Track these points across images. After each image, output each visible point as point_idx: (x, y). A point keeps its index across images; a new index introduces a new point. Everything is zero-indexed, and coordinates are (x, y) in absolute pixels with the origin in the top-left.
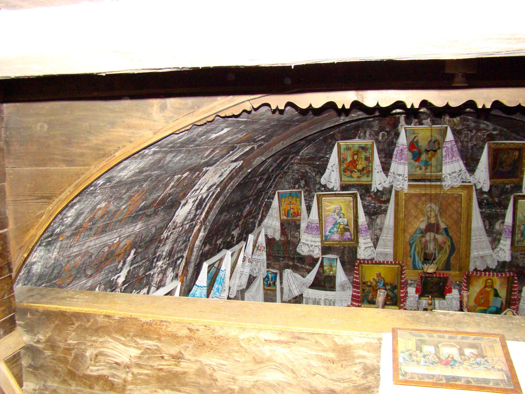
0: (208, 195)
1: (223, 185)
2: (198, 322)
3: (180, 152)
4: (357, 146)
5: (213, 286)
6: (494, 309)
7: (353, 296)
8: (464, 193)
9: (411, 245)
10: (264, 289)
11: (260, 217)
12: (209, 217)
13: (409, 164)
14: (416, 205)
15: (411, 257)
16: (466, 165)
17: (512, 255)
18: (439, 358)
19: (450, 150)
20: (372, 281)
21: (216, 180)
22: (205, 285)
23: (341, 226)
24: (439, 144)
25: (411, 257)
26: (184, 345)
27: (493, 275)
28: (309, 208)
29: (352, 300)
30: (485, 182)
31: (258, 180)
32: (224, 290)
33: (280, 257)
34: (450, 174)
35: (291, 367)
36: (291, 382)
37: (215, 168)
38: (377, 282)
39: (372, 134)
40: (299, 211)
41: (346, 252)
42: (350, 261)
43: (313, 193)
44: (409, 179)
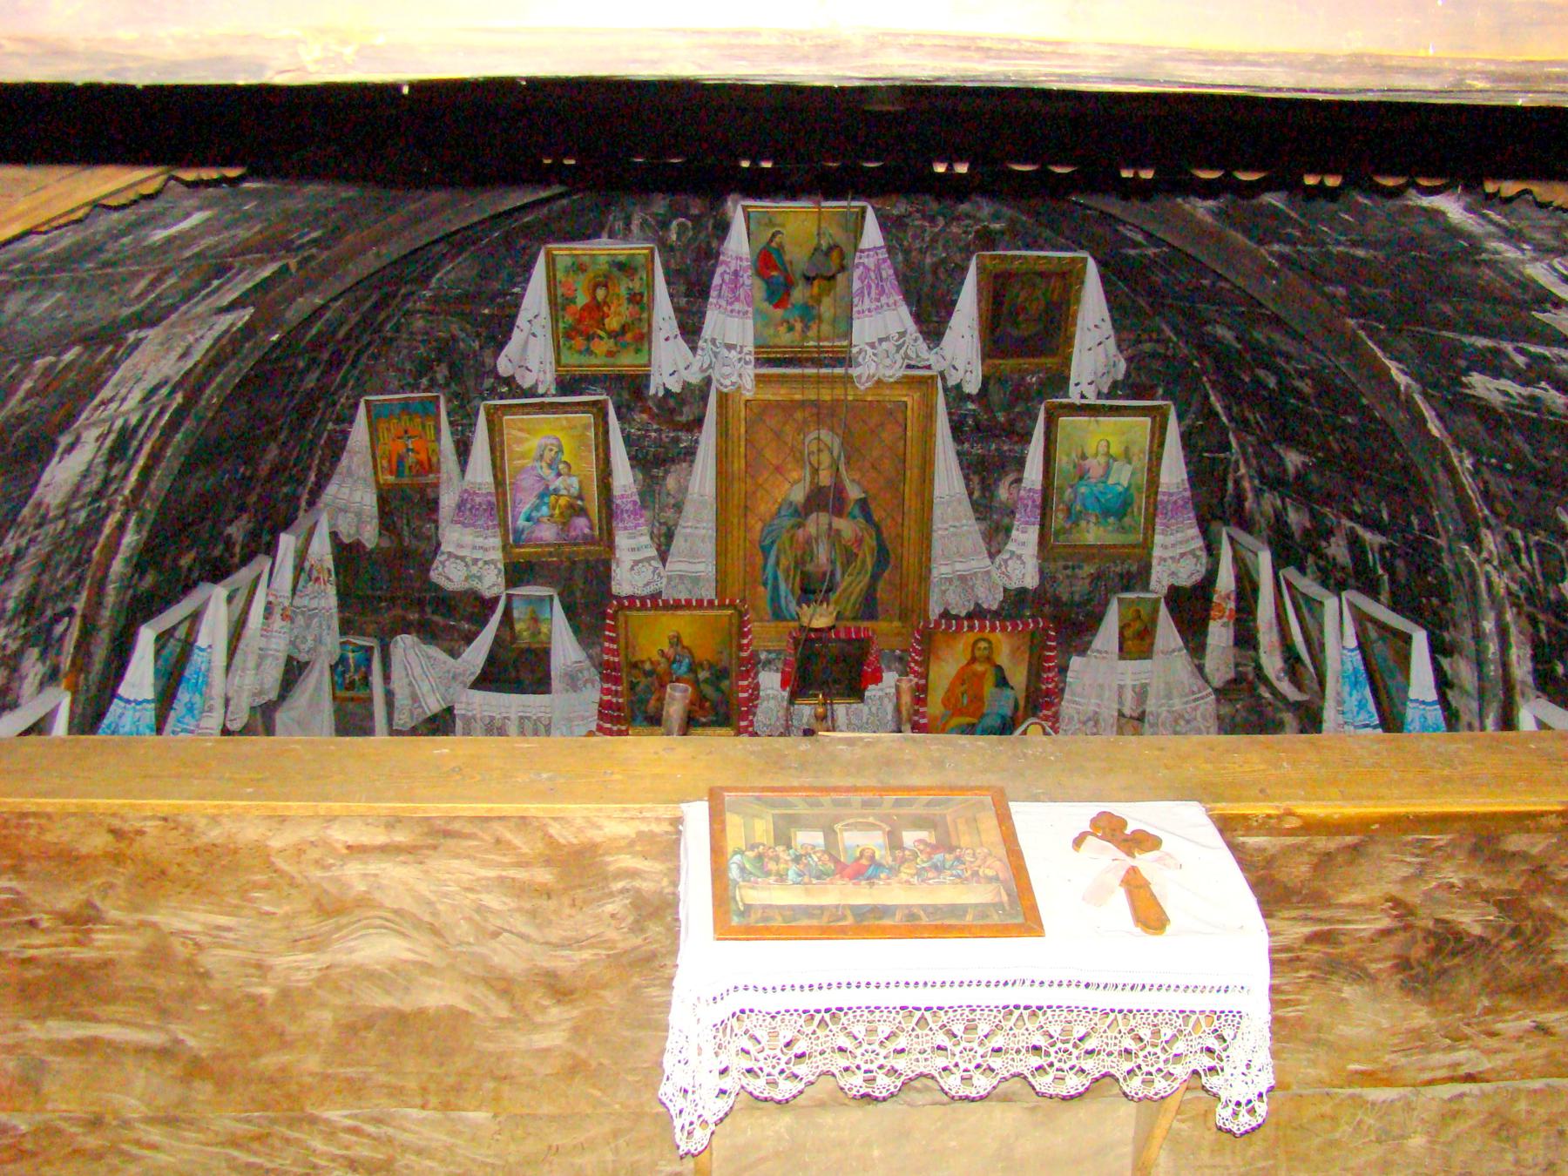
0: (144, 417)
1: (192, 385)
2: (145, 808)
3: (48, 285)
4: (603, 260)
5: (174, 697)
6: (995, 721)
7: (602, 704)
8: (911, 399)
9: (765, 553)
10: (335, 698)
11: (313, 478)
12: (152, 486)
13: (758, 313)
14: (778, 435)
15: (765, 584)
16: (918, 318)
17: (1041, 572)
18: (837, 861)
19: (873, 275)
20: (656, 657)
21: (170, 367)
22: (150, 695)
23: (563, 501)
24: (842, 255)
25: (765, 584)
26: (98, 881)
27: (993, 629)
28: (463, 449)
29: (601, 716)
30: (969, 368)
31: (301, 364)
32: (211, 709)
33: (380, 599)
34: (872, 345)
35: (427, 918)
36: (429, 960)
37: (165, 329)
38: (671, 662)
39: (650, 226)
40: (434, 460)
41: (578, 573)
42: (593, 604)
43: (475, 403)
44: (757, 360)
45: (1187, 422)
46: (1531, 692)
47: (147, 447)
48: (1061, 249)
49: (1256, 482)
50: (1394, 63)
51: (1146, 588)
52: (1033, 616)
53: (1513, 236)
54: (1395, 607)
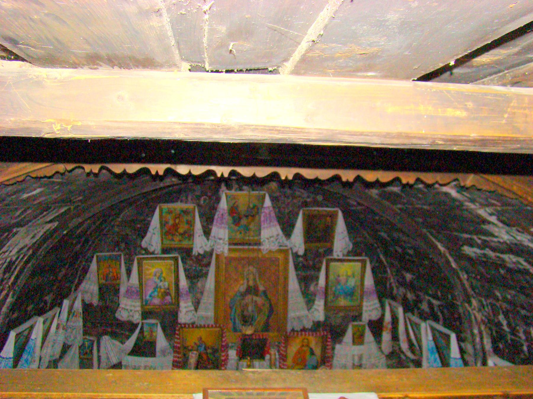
1: (36, 247)
7: (174, 361)
8: (280, 256)
9: (231, 308)
13: (230, 228)
16: (283, 230)
20: (193, 344)
21: (28, 241)
23: (162, 290)
24: (258, 209)
28: (129, 272)
34: (268, 239)
42: (171, 324)
43: (133, 256)
45: (373, 264)
46: (492, 354)
47: (18, 269)
48: (327, 207)
49: (397, 284)
50: (412, 135)
51: (360, 321)
52: (323, 330)
53: (473, 201)
54: (446, 325)
